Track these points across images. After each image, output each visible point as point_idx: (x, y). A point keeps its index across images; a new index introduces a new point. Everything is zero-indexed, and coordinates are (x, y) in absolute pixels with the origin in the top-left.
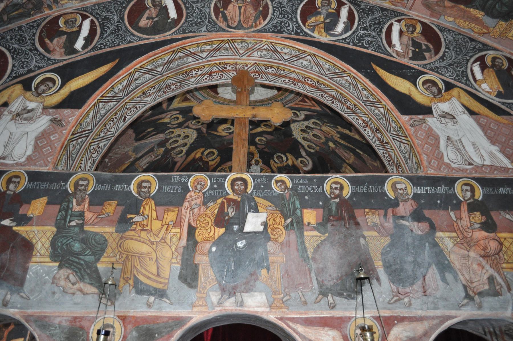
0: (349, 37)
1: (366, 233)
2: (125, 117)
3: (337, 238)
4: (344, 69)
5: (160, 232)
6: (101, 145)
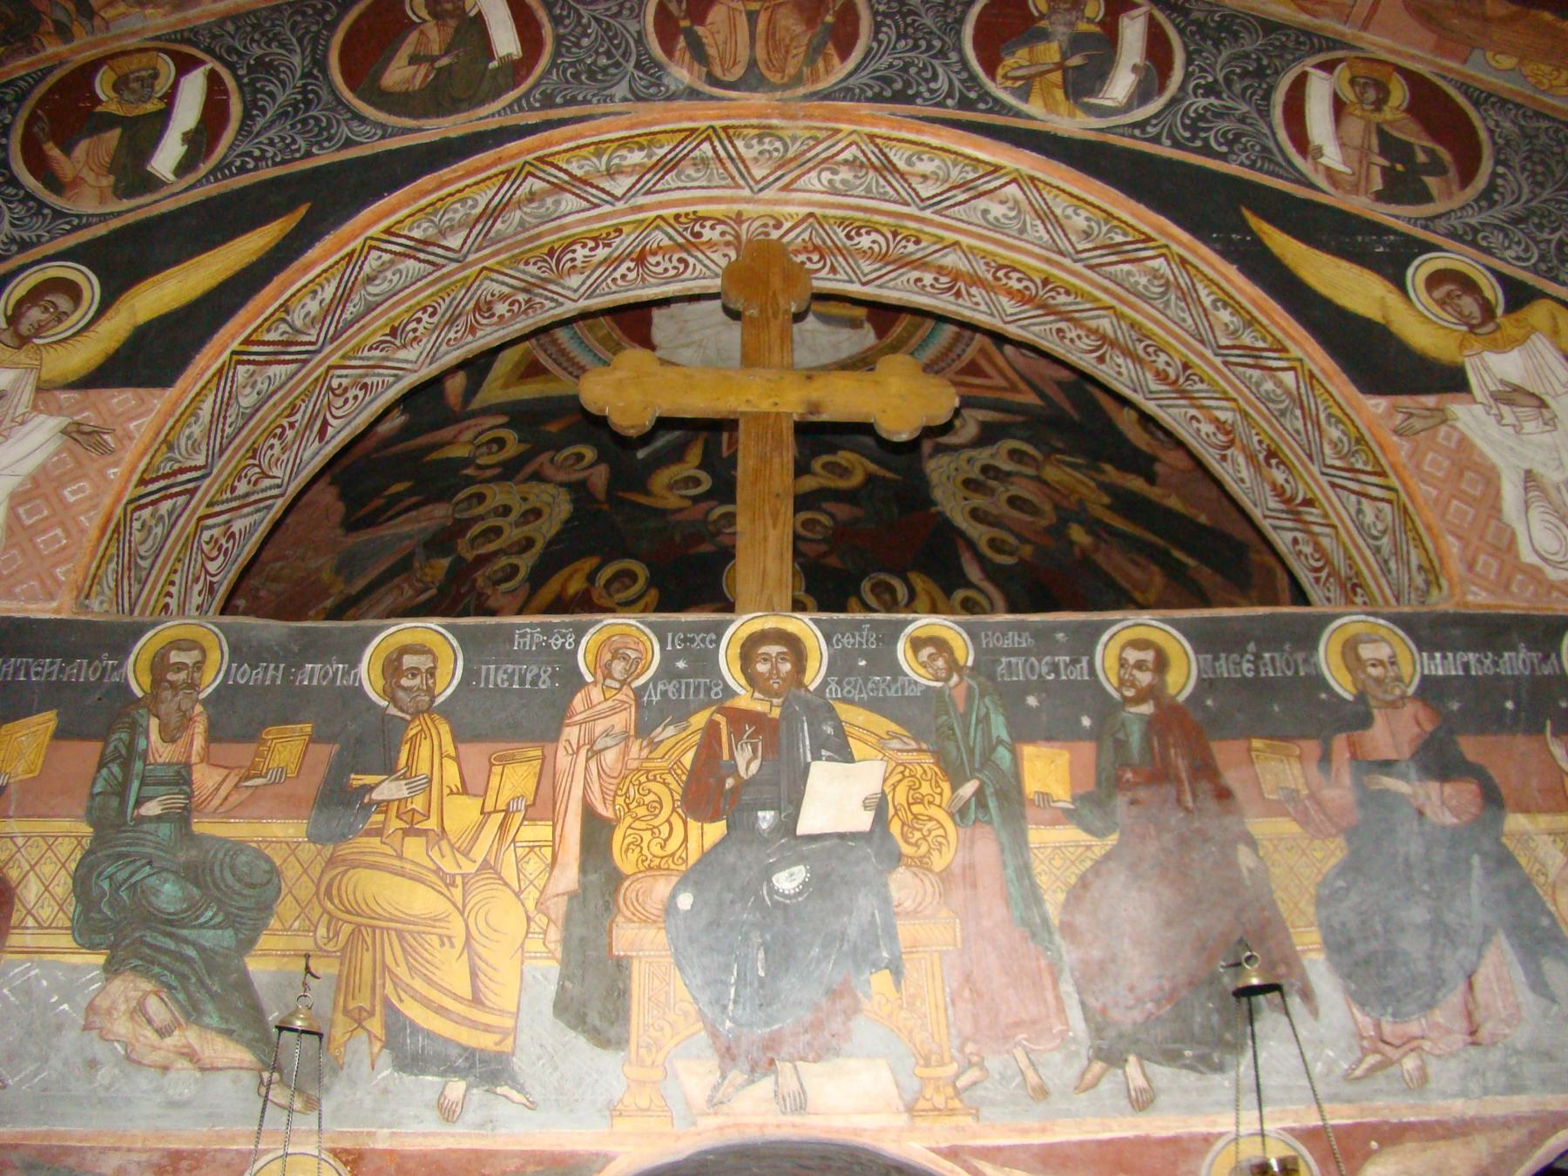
0: (1156, 116)
1: (1260, 827)
2: (325, 424)
3: (1152, 847)
4: (1146, 229)
5: (475, 839)
6: (238, 526)
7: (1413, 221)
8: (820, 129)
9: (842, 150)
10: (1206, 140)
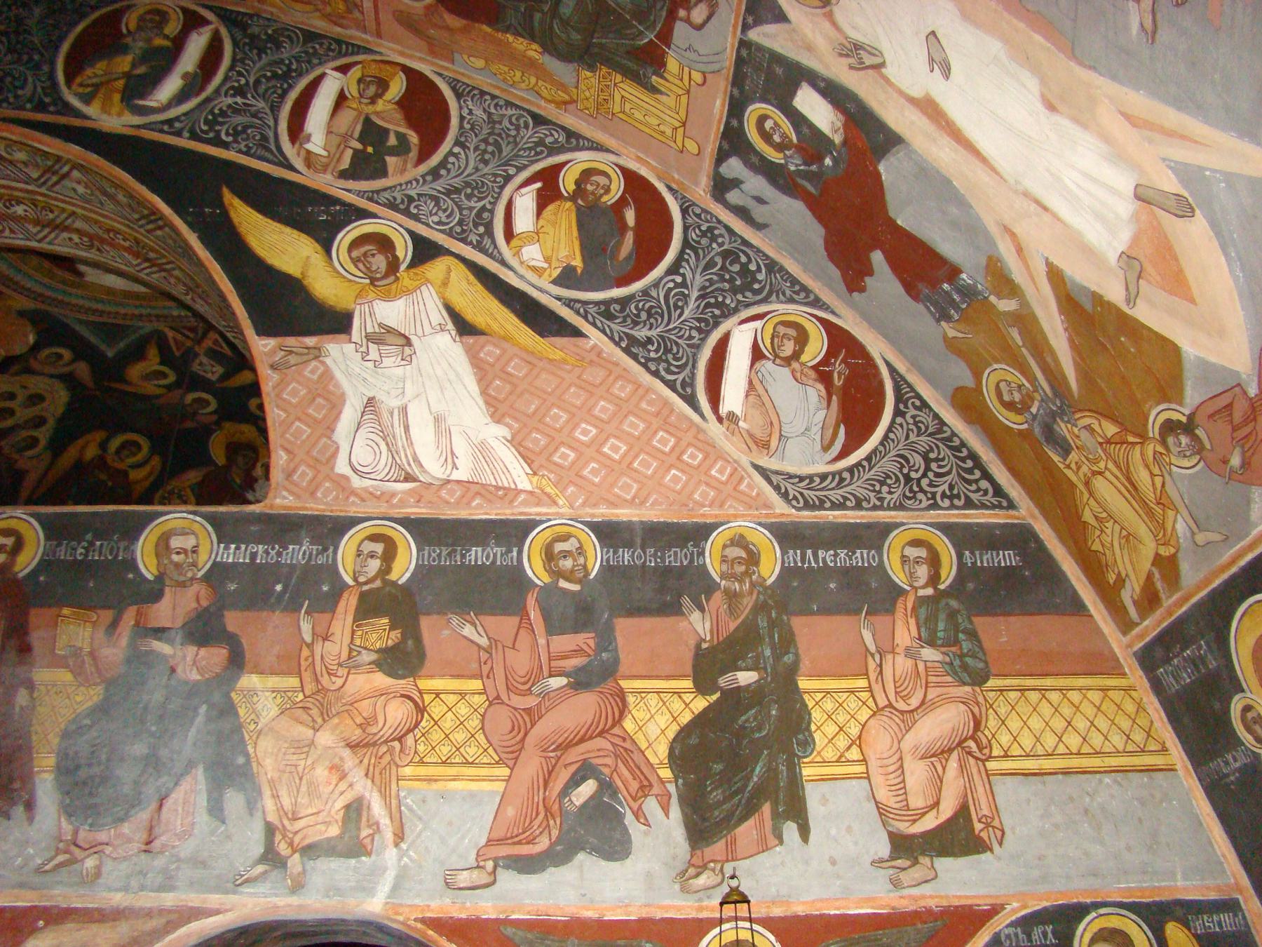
7: (360, 194)
10: (218, 133)
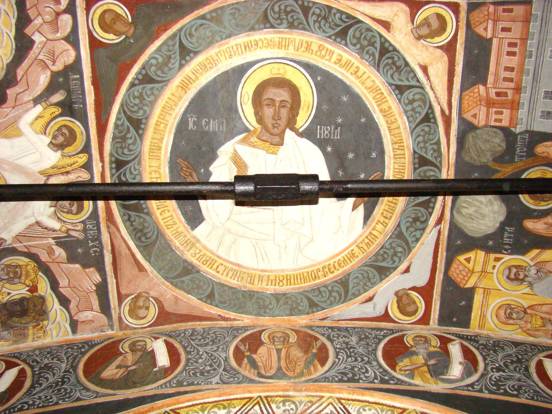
0: (477, 381)
8: (313, 396)
9: (325, 408)
10: (505, 389)
